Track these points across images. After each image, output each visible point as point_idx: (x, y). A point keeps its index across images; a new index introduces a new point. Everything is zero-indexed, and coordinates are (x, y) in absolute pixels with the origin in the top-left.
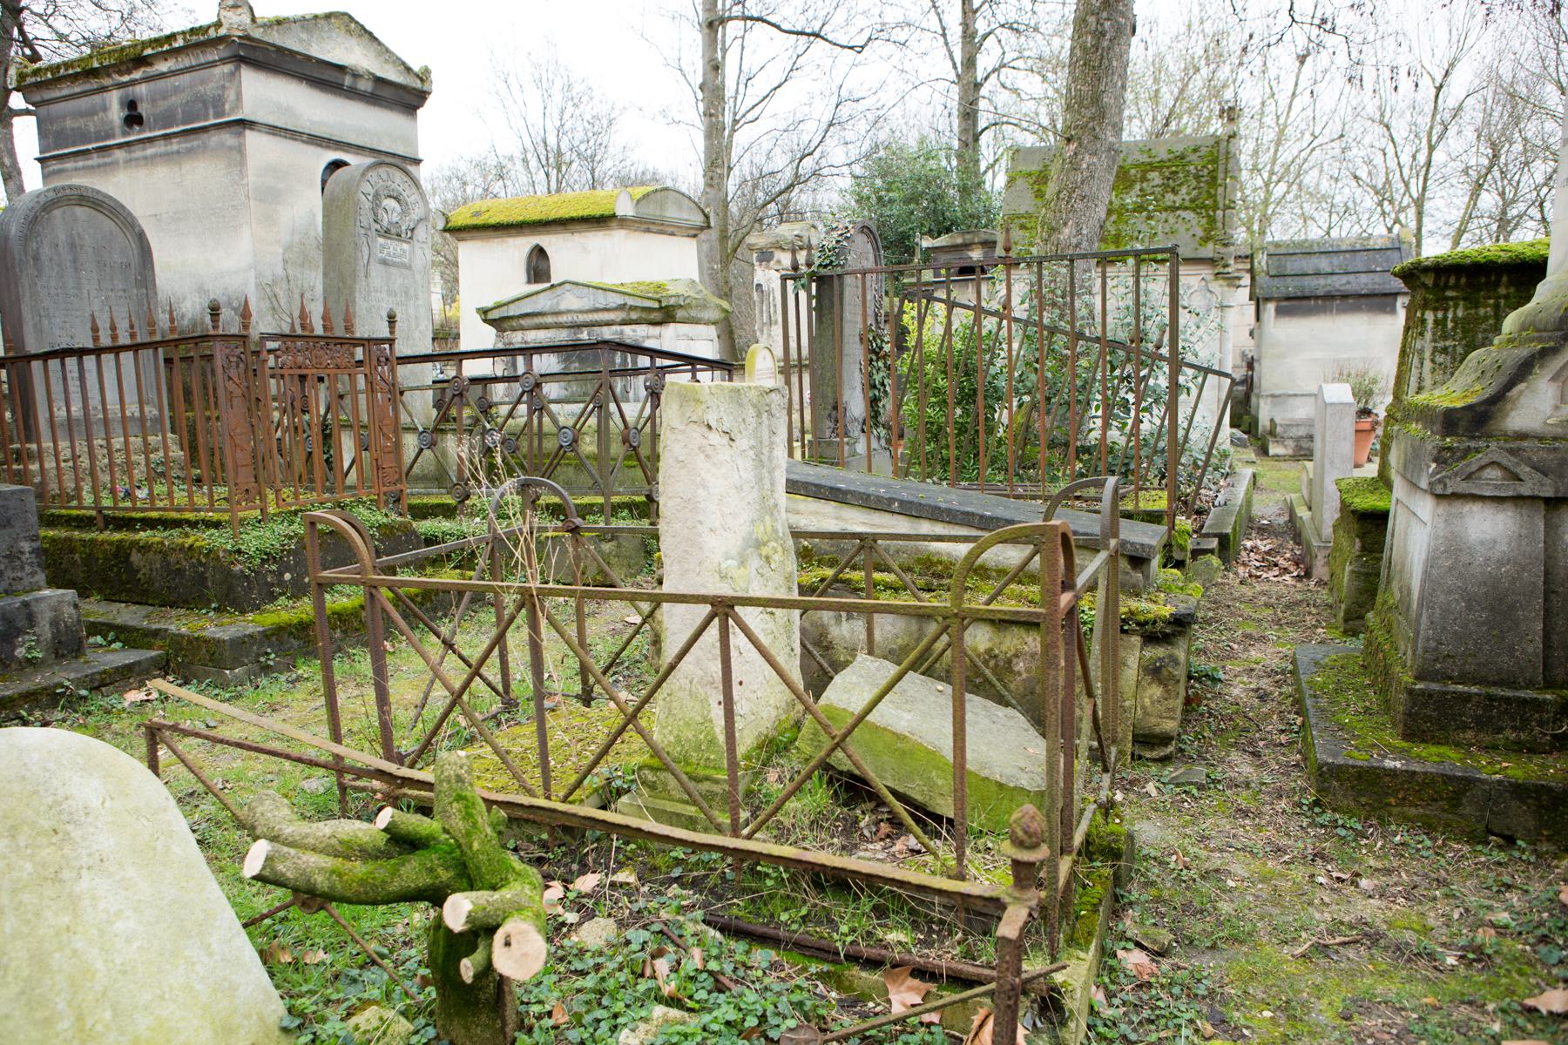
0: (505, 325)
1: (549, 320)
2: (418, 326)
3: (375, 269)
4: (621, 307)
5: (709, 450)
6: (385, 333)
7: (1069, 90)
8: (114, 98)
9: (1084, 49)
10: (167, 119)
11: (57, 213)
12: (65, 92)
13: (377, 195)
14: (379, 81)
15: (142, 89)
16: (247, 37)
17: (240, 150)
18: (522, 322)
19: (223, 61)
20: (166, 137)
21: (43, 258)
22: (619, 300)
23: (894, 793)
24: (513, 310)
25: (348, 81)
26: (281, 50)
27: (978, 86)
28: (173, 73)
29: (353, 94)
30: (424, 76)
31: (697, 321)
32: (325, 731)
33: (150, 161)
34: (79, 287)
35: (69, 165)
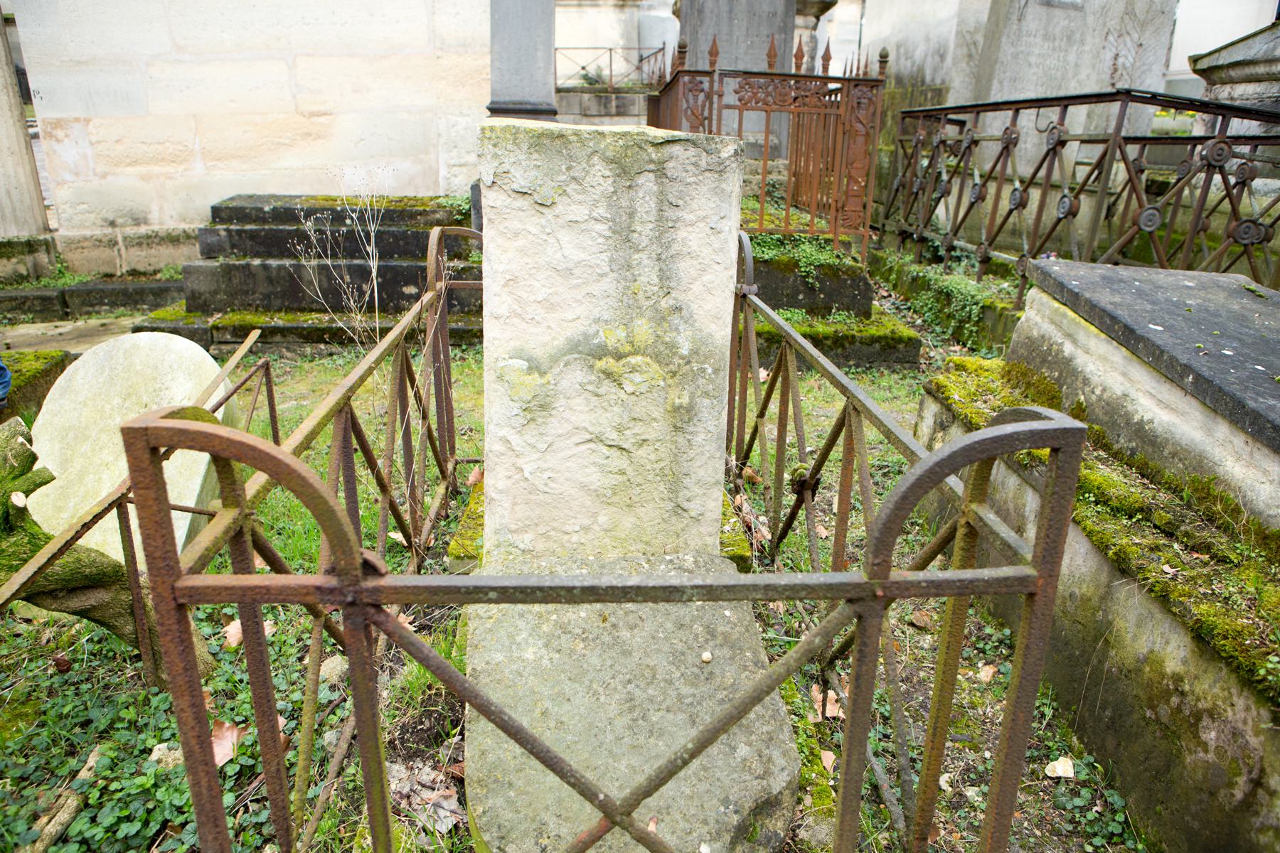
0: (1215, 77)
1: (1261, 70)
2: (1076, 75)
18: (1233, 73)
21: (707, 11)
23: (173, 415)
24: (1224, 59)
32: (911, 433)
34: (730, 34)
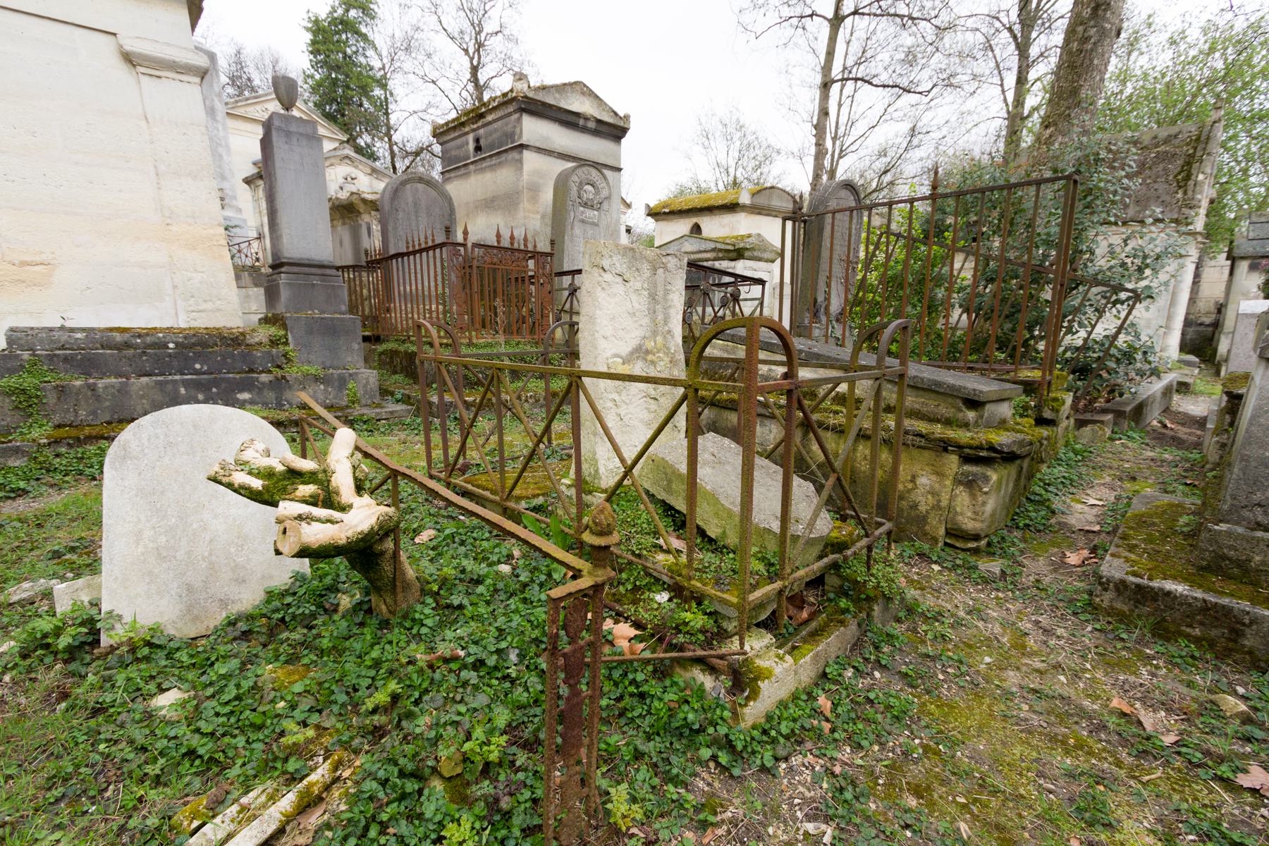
3: (577, 225)
4: (713, 250)
5: (604, 285)
6: (548, 250)
7: (1053, 87)
8: (471, 138)
9: (1070, 53)
10: (491, 147)
11: (408, 186)
12: (452, 136)
13: (581, 183)
14: (599, 122)
15: (482, 131)
16: (526, 97)
17: (520, 161)
19: (515, 112)
20: (491, 156)
22: (712, 245)
25: (581, 122)
26: (544, 104)
27: (1023, 119)
28: (494, 121)
29: (584, 130)
30: (627, 117)
31: (760, 259)
33: (482, 170)
35: (452, 175)
